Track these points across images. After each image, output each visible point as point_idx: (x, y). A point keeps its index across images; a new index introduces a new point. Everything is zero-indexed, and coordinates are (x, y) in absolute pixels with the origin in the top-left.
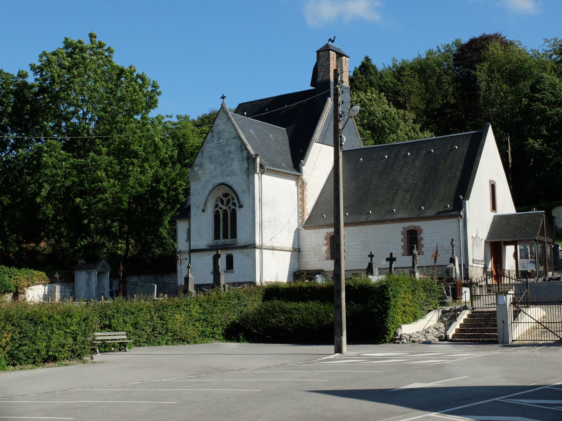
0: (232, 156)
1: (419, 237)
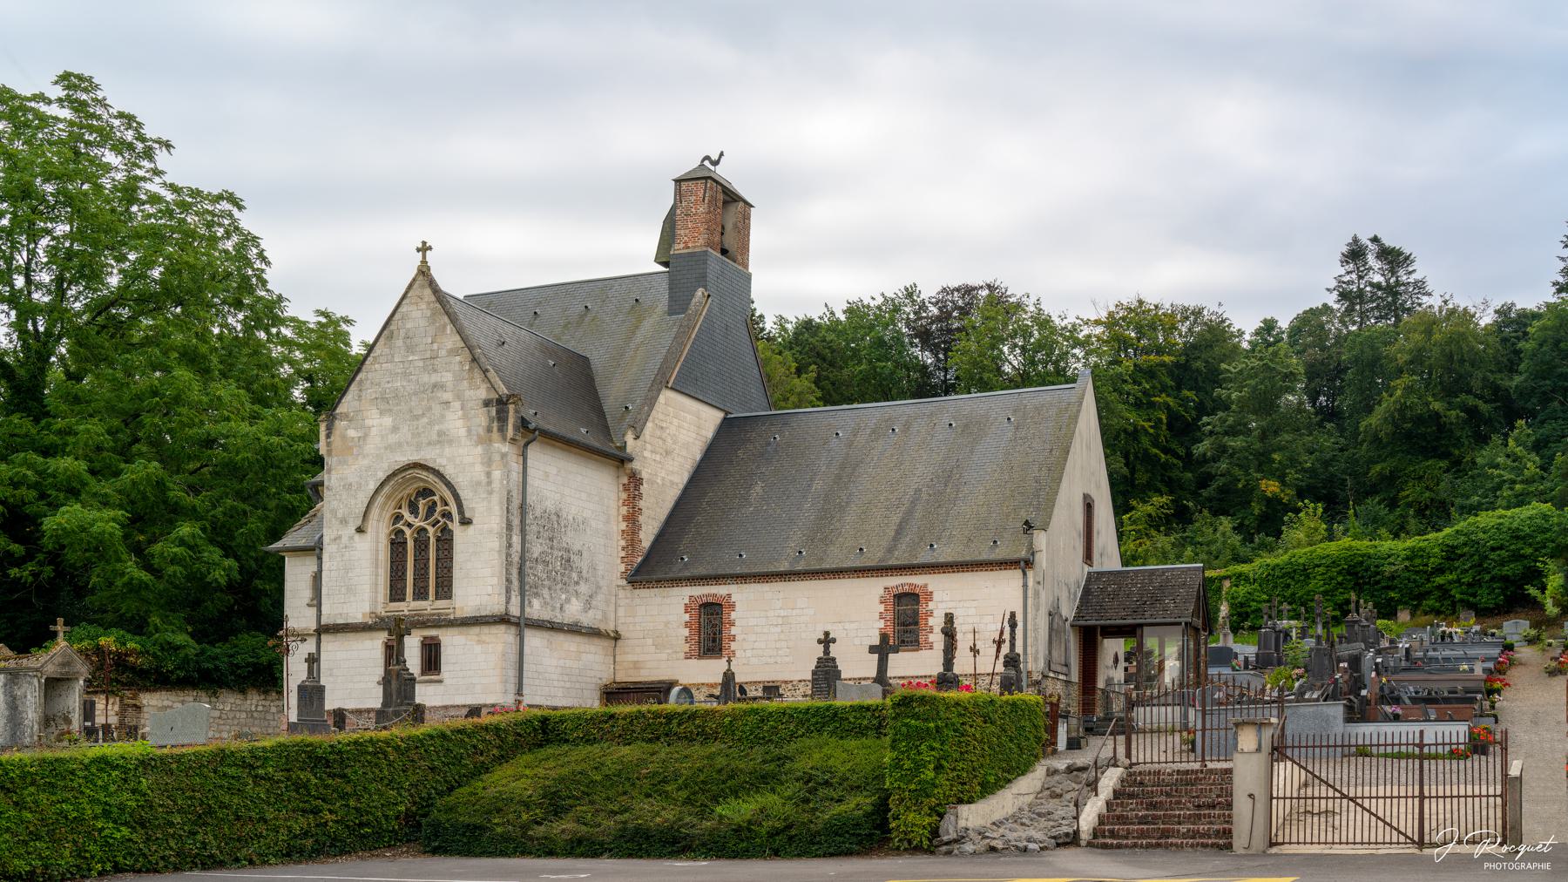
1: (922, 610)
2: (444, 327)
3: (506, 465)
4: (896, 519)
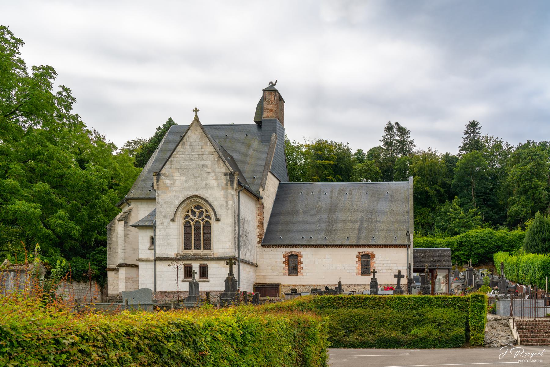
1: (371, 261)
2: (207, 143)
3: (234, 199)
4: (357, 227)
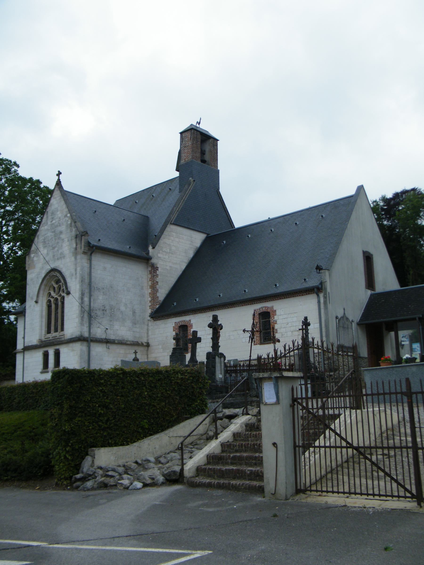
0: (63, 236)
1: (272, 321)
